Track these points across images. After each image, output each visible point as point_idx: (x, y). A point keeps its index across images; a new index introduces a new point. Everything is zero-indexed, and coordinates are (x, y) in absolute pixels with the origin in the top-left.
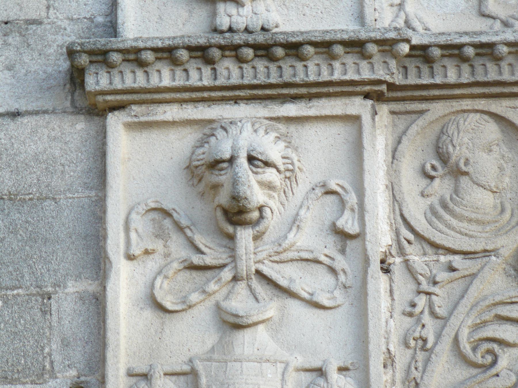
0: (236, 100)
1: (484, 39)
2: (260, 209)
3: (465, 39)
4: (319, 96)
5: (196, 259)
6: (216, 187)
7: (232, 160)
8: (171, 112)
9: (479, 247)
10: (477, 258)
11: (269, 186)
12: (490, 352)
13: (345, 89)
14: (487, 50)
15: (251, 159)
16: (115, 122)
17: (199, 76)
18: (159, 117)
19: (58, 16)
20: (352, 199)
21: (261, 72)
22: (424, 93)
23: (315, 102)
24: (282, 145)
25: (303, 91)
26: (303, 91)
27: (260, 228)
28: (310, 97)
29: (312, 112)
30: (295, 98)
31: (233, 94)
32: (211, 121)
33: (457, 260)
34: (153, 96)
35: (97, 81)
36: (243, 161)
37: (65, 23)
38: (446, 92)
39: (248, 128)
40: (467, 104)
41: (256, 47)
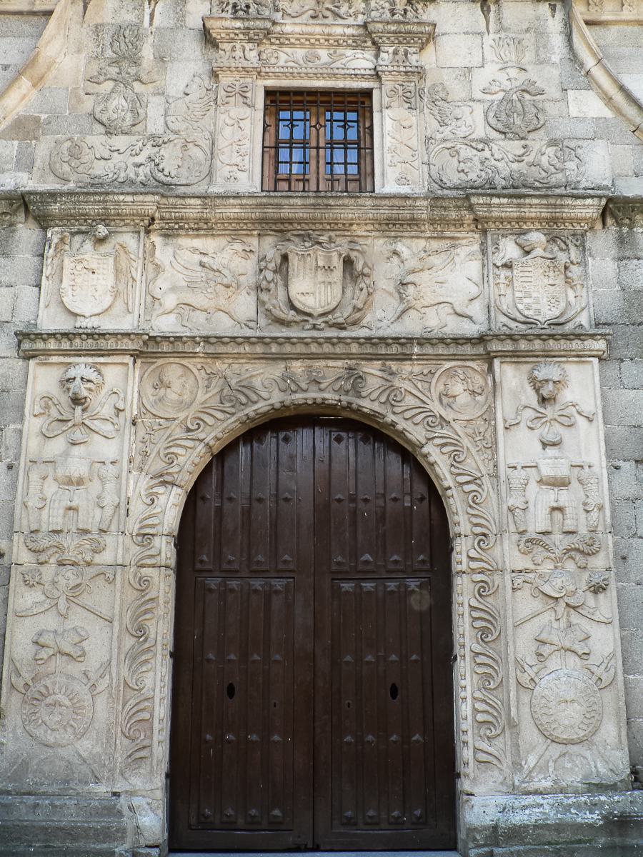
0: (80, 355)
1: (178, 335)
2: (85, 398)
3: (171, 335)
4: (113, 355)
5: (60, 418)
6: (69, 389)
7: (74, 379)
8: (54, 359)
9: (171, 417)
10: (458, 189)
11: (90, 390)
12: (198, 424)
13: (123, 352)
14: (179, 338)
15: (82, 379)
16: (32, 363)
17: (66, 345)
18: (50, 361)
19: (16, 320)
20: (122, 396)
21: (90, 344)
22: (503, 354)
23: (111, 357)
24: (96, 373)
25: (106, 353)
26: (106, 353)
27: (86, 405)
28: (109, 355)
29: (110, 361)
30: (102, 355)
31: (79, 353)
32: (70, 363)
33: (162, 421)
34: (47, 353)
35: (26, 345)
36: (78, 379)
37: (18, 323)
38: (163, 355)
39: (82, 367)
40: (172, 360)
41: (88, 334)
